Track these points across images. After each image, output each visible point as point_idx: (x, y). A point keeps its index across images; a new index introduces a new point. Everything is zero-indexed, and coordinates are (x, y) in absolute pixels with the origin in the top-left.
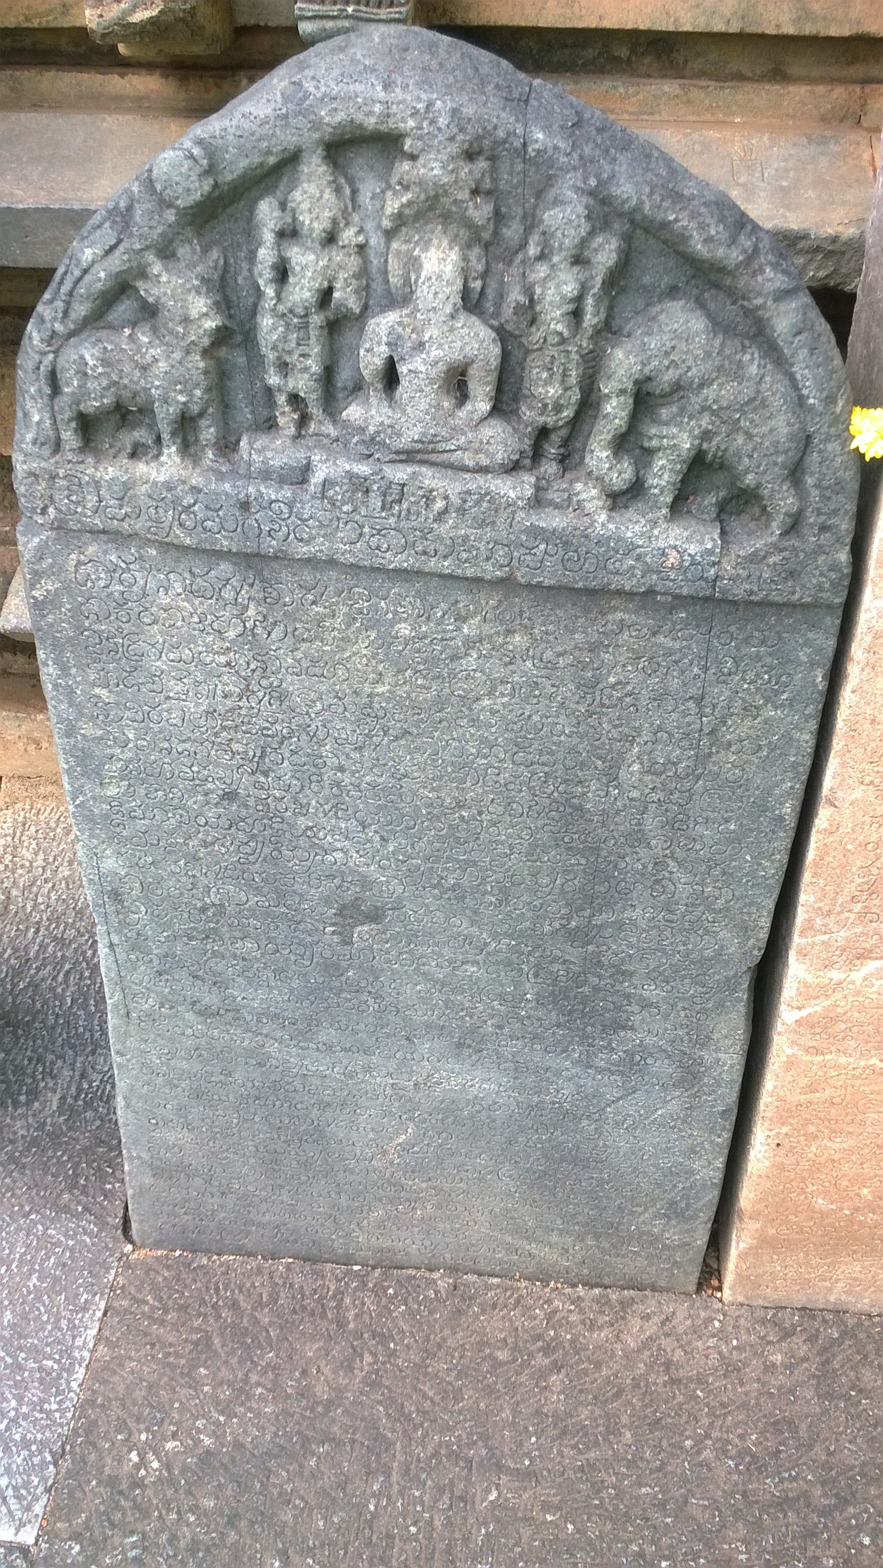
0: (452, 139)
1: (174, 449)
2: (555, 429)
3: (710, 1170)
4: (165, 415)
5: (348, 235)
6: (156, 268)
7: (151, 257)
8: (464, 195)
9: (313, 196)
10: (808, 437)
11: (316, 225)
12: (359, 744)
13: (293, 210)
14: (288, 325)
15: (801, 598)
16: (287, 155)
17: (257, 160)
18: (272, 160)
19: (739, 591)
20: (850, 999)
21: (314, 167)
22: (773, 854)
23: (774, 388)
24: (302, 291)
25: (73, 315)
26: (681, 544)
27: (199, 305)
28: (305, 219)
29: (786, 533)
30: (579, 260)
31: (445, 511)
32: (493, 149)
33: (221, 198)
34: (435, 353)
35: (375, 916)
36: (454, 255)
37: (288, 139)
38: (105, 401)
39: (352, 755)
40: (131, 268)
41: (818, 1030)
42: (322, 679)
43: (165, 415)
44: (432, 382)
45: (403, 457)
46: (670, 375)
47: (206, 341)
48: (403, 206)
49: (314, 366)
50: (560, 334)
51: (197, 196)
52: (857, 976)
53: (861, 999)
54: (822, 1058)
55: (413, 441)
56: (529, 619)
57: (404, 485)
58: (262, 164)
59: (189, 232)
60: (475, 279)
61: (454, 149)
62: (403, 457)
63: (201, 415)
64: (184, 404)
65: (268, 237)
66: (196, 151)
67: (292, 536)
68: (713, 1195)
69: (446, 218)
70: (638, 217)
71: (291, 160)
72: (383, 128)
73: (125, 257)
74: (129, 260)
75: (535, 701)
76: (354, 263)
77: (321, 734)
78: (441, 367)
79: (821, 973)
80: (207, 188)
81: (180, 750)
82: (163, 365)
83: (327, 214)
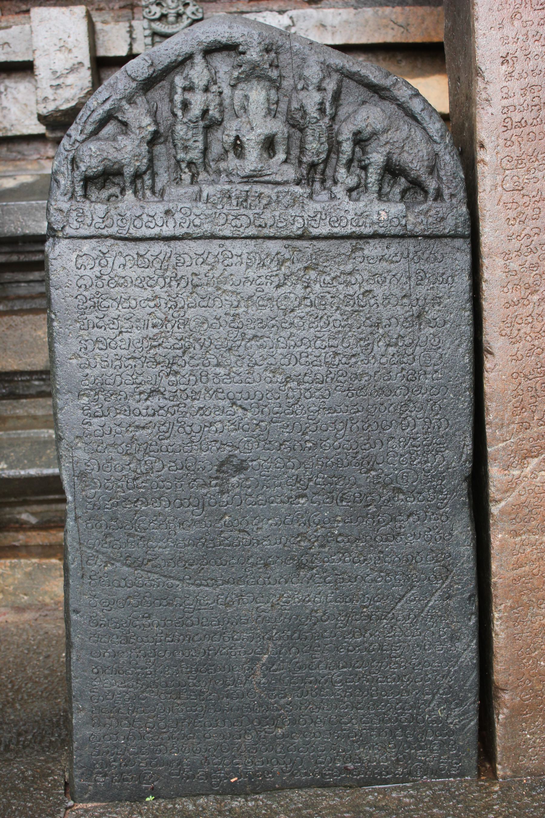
0: (260, 43)
1: (131, 191)
2: (318, 164)
3: (467, 651)
4: (129, 171)
5: (214, 88)
6: (127, 106)
7: (124, 103)
8: (267, 66)
9: (198, 73)
10: (437, 154)
11: (200, 83)
12: (229, 347)
13: (190, 78)
14: (188, 127)
15: (449, 232)
16: (187, 56)
17: (174, 58)
18: (180, 59)
19: (418, 229)
20: (527, 489)
21: (198, 58)
22: (465, 392)
23: (418, 135)
24: (196, 111)
25: (86, 132)
26: (386, 212)
27: (147, 120)
28: (196, 81)
29: (435, 200)
30: (320, 89)
31: (269, 203)
32: (277, 49)
33: (156, 77)
34: (259, 131)
35: (241, 468)
36: (264, 93)
37: (187, 49)
38: (99, 168)
39: (225, 354)
40: (114, 108)
41: (513, 516)
42: (208, 308)
43: (129, 171)
44: (258, 143)
45: (245, 180)
46: (369, 129)
47: (149, 137)
48: (240, 74)
49: (200, 145)
50: (316, 118)
51: (146, 75)
52: (527, 470)
53: (533, 488)
54: (520, 538)
55: (251, 171)
56: (315, 259)
57: (247, 191)
58: (176, 60)
59: (141, 92)
60: (273, 104)
61: (262, 47)
62: (245, 180)
63: (145, 173)
64: (138, 166)
65: (179, 90)
66: (147, 58)
67: (192, 224)
68: (474, 676)
69: (259, 78)
70: (345, 71)
71: (190, 57)
72: (230, 43)
73: (113, 103)
74: (114, 104)
75: (322, 307)
76: (217, 100)
77: (207, 344)
78: (263, 137)
79: (506, 472)
80: (151, 72)
81: (126, 365)
82: (129, 148)
83: (206, 78)
